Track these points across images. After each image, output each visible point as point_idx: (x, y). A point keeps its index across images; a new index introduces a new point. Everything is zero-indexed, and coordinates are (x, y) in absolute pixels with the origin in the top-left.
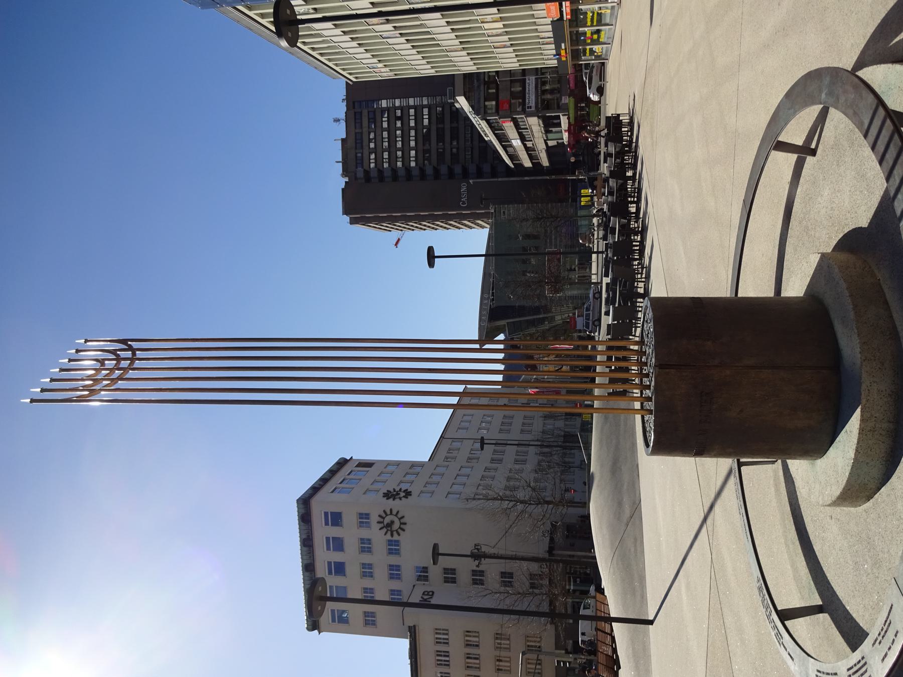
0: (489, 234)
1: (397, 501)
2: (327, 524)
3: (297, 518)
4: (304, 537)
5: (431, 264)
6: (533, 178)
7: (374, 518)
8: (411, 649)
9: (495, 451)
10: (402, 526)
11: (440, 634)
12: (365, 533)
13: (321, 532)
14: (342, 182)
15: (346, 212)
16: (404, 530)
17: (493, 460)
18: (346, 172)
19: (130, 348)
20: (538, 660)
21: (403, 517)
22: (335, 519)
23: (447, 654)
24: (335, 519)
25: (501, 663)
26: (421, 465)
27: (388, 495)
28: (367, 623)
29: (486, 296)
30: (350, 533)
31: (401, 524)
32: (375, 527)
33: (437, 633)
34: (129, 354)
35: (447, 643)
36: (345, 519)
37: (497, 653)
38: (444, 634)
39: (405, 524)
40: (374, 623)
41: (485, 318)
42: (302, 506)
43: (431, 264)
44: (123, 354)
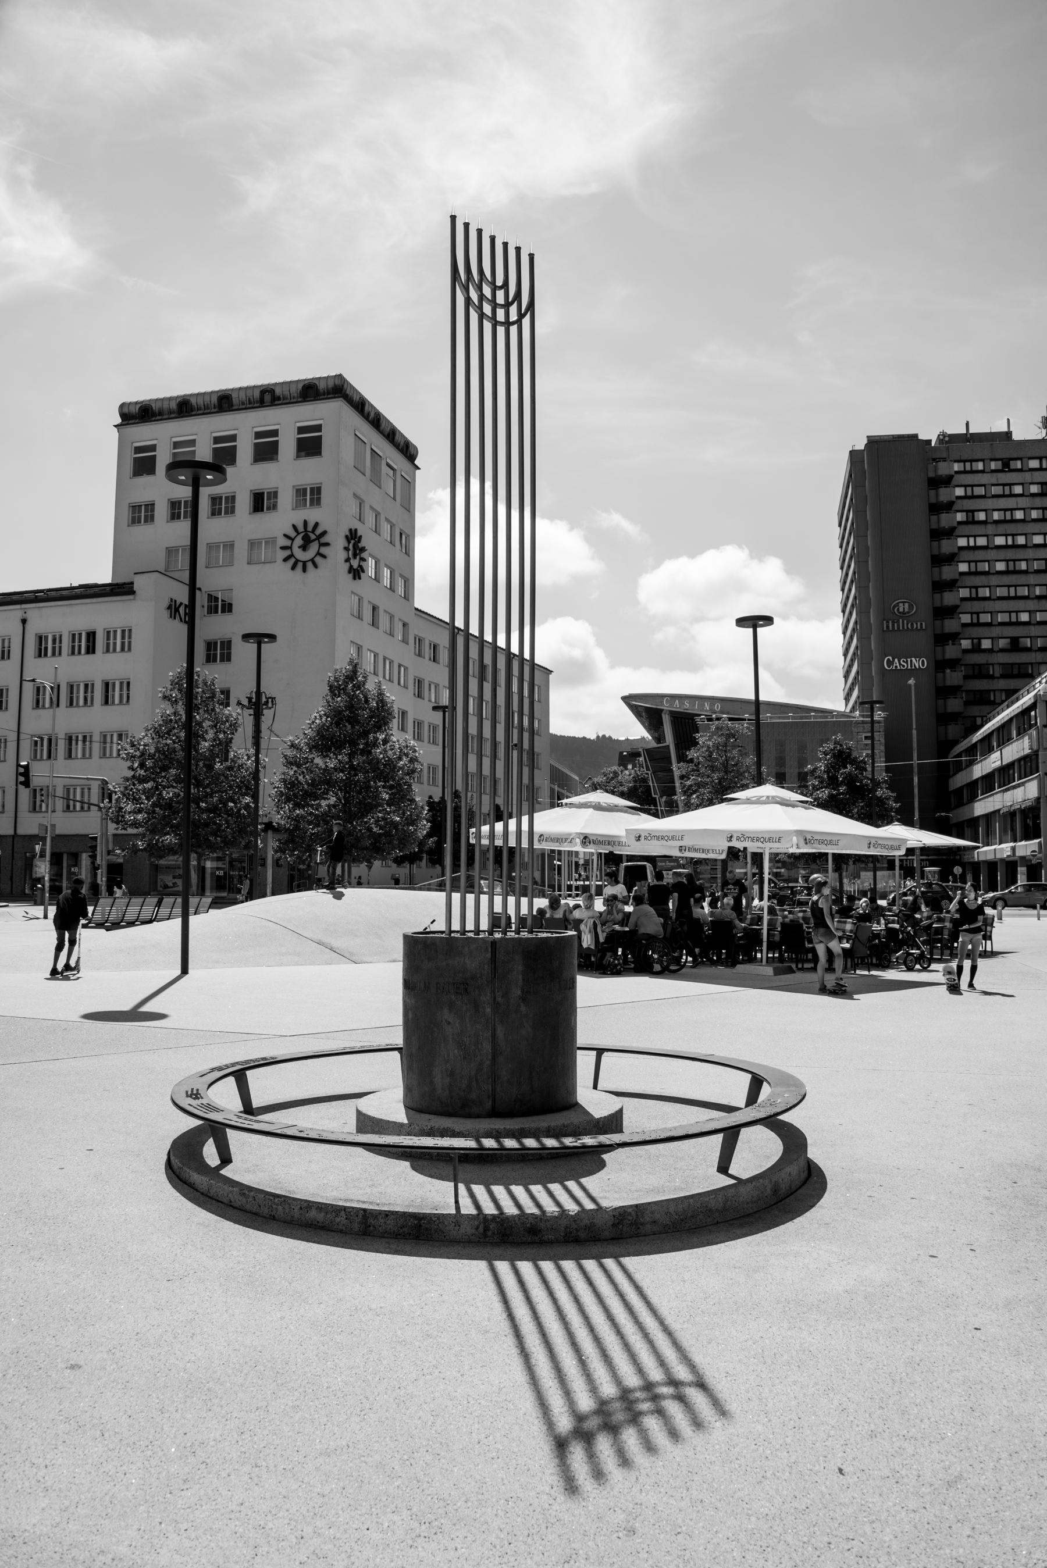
0: (830, 712)
1: (343, 555)
2: (301, 430)
3: (310, 377)
4: (278, 391)
5: (742, 622)
6: (916, 791)
7: (312, 515)
8: (96, 586)
9: (435, 728)
10: (300, 565)
11: (123, 637)
12: (286, 499)
13: (285, 422)
14: (929, 433)
15: (874, 442)
16: (293, 568)
17: (418, 724)
18: (948, 440)
19: (521, 316)
20: (90, 804)
21: (316, 566)
22: (310, 445)
23: (91, 649)
24: (310, 445)
25: (80, 743)
26: (408, 595)
27: (353, 536)
28: (135, 508)
29: (718, 707)
30: (286, 473)
31: (304, 563)
32: (298, 517)
33: (123, 632)
34: (513, 317)
35: (108, 651)
36: (310, 463)
37: (96, 737)
38: (123, 644)
39: (304, 570)
40: (135, 521)
41: (677, 706)
42: (331, 384)
43: (742, 622)
44: (513, 309)
